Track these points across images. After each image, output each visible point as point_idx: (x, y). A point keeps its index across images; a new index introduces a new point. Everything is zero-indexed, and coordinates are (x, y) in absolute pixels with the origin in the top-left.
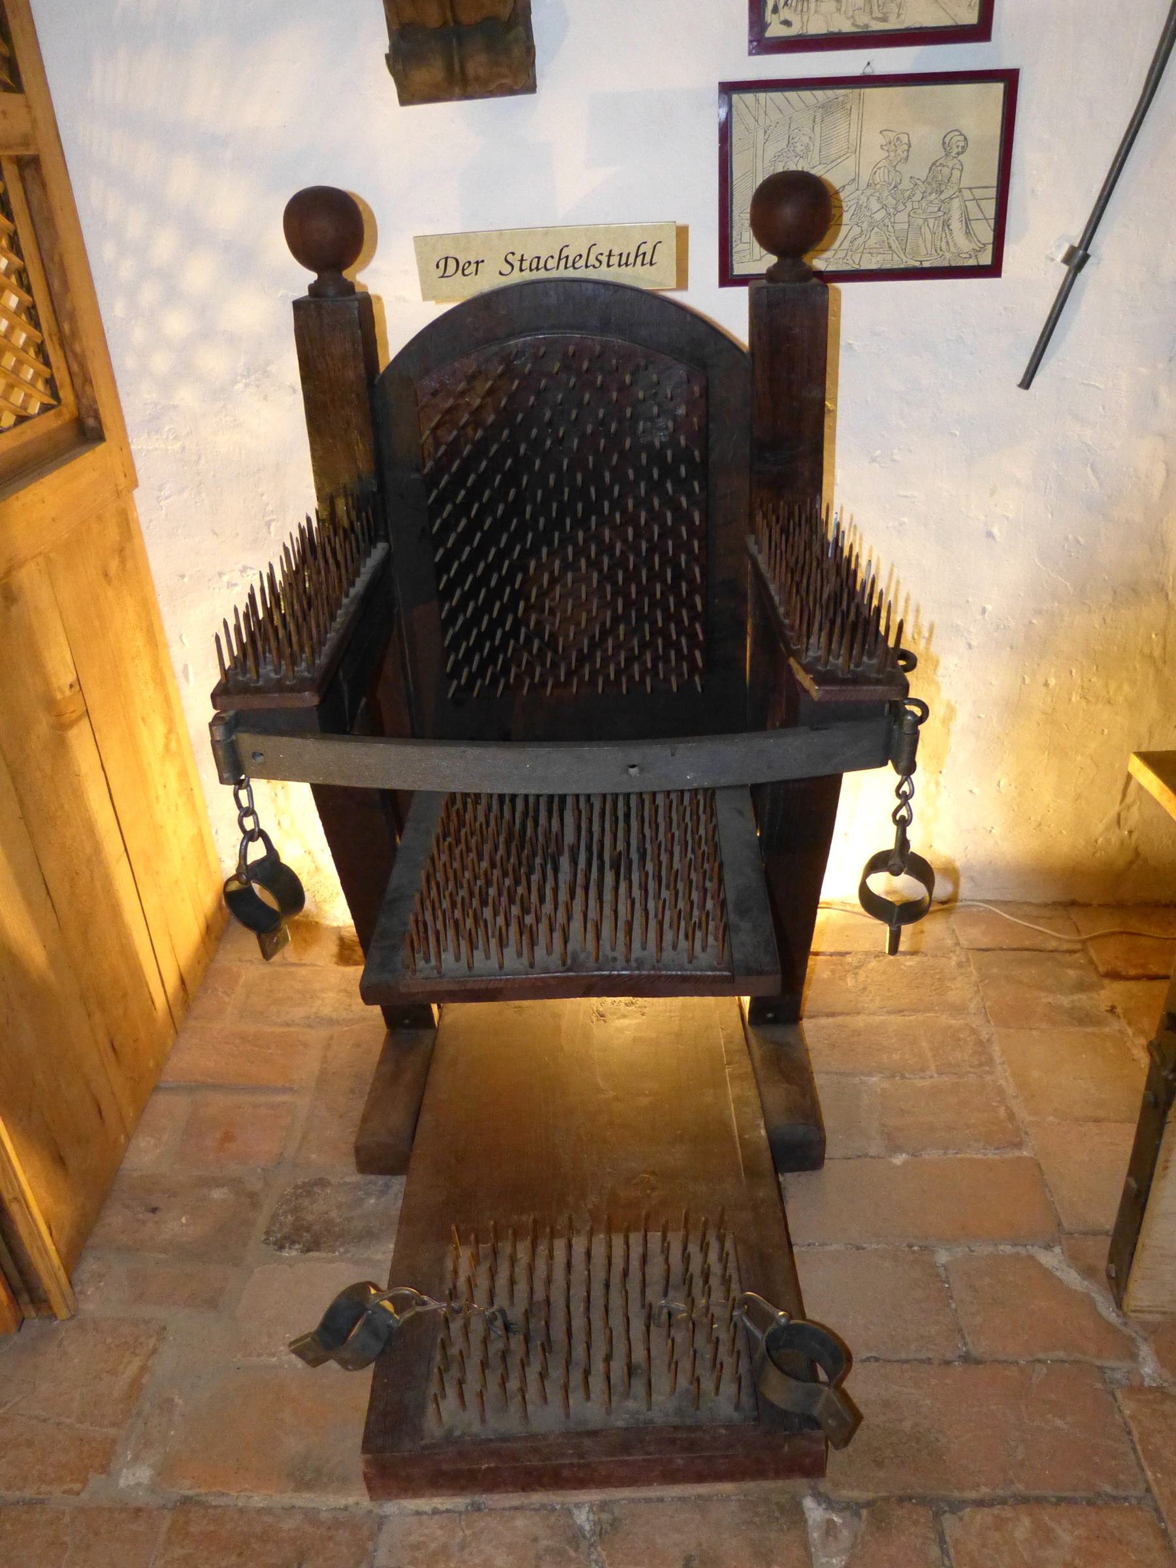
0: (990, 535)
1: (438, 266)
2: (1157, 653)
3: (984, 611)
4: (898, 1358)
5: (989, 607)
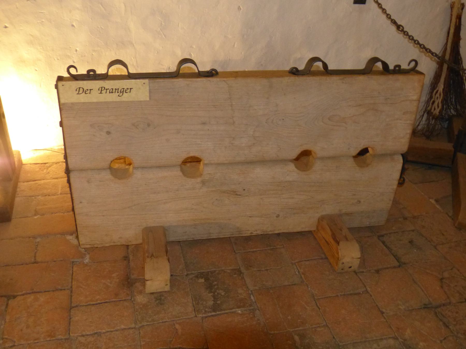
0: (73, 26)
1: (76, 90)
2: (135, 64)
3: (76, 51)
4: (132, 330)
5: (78, 49)
